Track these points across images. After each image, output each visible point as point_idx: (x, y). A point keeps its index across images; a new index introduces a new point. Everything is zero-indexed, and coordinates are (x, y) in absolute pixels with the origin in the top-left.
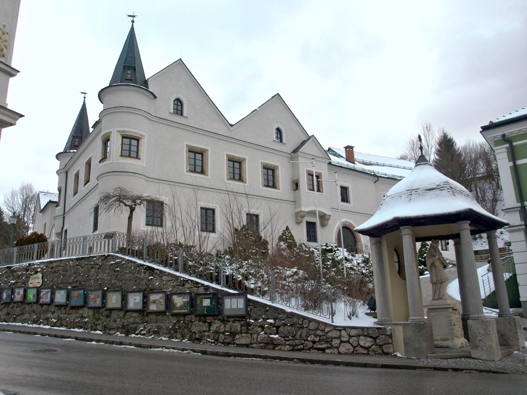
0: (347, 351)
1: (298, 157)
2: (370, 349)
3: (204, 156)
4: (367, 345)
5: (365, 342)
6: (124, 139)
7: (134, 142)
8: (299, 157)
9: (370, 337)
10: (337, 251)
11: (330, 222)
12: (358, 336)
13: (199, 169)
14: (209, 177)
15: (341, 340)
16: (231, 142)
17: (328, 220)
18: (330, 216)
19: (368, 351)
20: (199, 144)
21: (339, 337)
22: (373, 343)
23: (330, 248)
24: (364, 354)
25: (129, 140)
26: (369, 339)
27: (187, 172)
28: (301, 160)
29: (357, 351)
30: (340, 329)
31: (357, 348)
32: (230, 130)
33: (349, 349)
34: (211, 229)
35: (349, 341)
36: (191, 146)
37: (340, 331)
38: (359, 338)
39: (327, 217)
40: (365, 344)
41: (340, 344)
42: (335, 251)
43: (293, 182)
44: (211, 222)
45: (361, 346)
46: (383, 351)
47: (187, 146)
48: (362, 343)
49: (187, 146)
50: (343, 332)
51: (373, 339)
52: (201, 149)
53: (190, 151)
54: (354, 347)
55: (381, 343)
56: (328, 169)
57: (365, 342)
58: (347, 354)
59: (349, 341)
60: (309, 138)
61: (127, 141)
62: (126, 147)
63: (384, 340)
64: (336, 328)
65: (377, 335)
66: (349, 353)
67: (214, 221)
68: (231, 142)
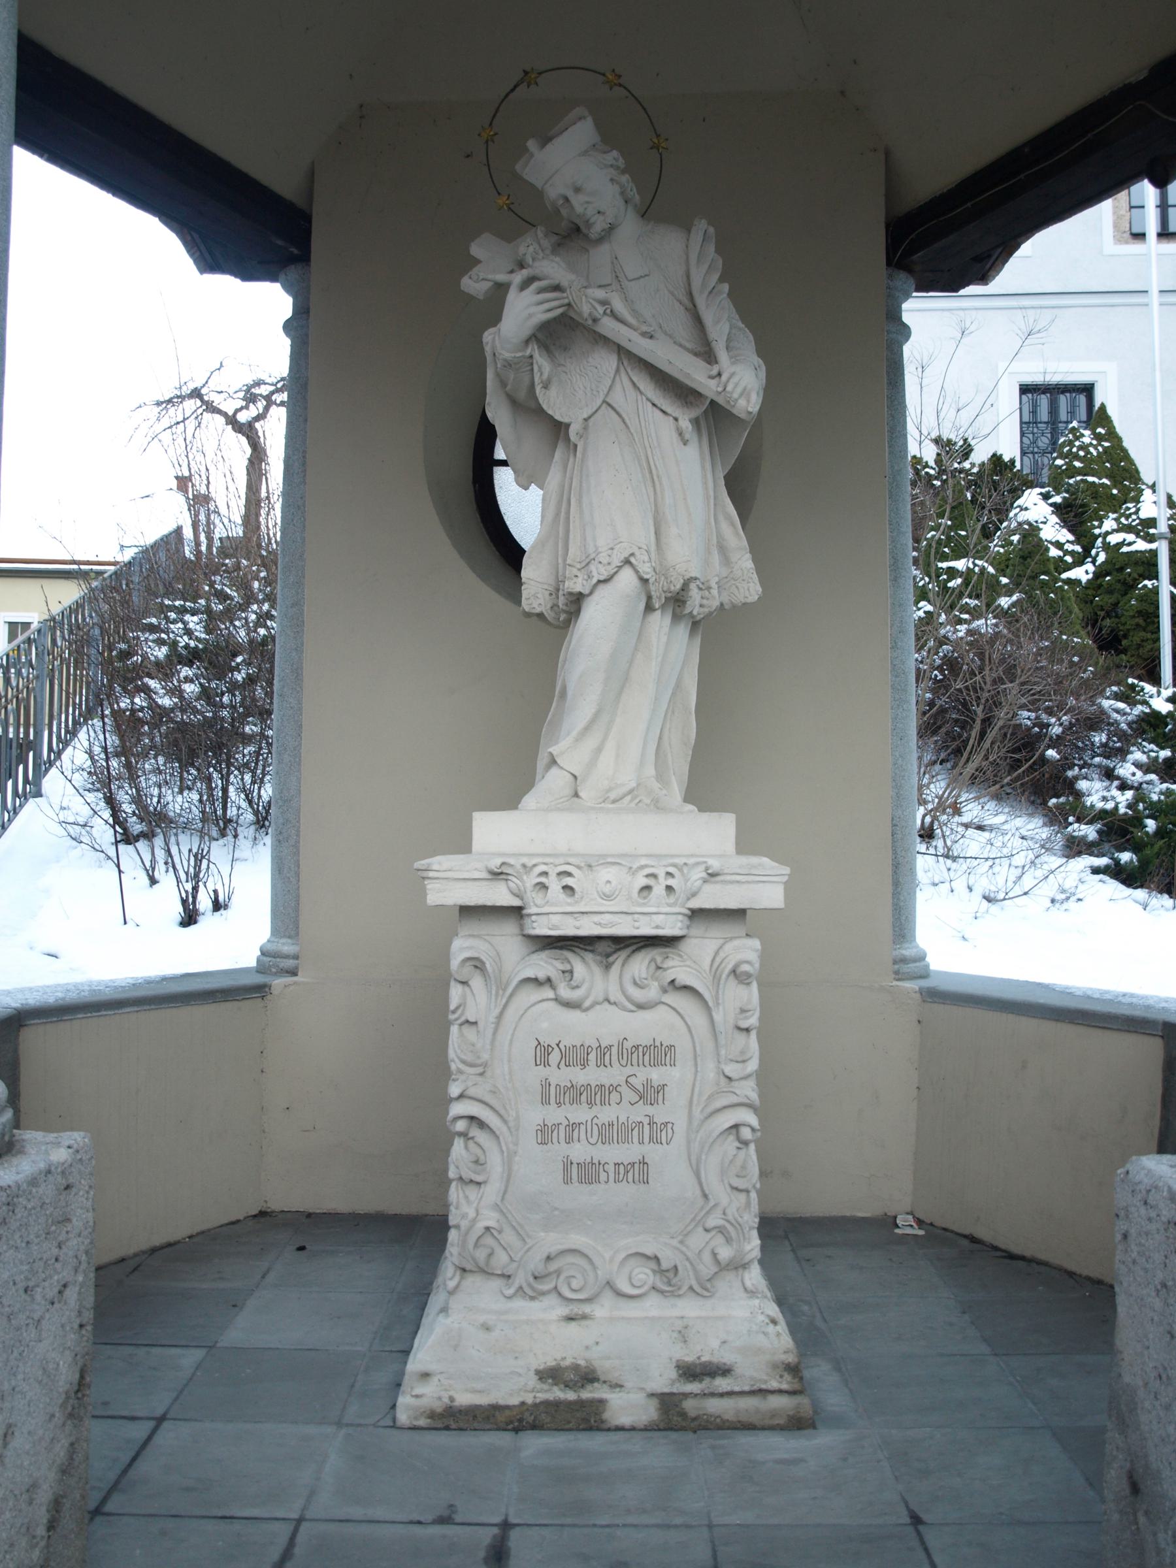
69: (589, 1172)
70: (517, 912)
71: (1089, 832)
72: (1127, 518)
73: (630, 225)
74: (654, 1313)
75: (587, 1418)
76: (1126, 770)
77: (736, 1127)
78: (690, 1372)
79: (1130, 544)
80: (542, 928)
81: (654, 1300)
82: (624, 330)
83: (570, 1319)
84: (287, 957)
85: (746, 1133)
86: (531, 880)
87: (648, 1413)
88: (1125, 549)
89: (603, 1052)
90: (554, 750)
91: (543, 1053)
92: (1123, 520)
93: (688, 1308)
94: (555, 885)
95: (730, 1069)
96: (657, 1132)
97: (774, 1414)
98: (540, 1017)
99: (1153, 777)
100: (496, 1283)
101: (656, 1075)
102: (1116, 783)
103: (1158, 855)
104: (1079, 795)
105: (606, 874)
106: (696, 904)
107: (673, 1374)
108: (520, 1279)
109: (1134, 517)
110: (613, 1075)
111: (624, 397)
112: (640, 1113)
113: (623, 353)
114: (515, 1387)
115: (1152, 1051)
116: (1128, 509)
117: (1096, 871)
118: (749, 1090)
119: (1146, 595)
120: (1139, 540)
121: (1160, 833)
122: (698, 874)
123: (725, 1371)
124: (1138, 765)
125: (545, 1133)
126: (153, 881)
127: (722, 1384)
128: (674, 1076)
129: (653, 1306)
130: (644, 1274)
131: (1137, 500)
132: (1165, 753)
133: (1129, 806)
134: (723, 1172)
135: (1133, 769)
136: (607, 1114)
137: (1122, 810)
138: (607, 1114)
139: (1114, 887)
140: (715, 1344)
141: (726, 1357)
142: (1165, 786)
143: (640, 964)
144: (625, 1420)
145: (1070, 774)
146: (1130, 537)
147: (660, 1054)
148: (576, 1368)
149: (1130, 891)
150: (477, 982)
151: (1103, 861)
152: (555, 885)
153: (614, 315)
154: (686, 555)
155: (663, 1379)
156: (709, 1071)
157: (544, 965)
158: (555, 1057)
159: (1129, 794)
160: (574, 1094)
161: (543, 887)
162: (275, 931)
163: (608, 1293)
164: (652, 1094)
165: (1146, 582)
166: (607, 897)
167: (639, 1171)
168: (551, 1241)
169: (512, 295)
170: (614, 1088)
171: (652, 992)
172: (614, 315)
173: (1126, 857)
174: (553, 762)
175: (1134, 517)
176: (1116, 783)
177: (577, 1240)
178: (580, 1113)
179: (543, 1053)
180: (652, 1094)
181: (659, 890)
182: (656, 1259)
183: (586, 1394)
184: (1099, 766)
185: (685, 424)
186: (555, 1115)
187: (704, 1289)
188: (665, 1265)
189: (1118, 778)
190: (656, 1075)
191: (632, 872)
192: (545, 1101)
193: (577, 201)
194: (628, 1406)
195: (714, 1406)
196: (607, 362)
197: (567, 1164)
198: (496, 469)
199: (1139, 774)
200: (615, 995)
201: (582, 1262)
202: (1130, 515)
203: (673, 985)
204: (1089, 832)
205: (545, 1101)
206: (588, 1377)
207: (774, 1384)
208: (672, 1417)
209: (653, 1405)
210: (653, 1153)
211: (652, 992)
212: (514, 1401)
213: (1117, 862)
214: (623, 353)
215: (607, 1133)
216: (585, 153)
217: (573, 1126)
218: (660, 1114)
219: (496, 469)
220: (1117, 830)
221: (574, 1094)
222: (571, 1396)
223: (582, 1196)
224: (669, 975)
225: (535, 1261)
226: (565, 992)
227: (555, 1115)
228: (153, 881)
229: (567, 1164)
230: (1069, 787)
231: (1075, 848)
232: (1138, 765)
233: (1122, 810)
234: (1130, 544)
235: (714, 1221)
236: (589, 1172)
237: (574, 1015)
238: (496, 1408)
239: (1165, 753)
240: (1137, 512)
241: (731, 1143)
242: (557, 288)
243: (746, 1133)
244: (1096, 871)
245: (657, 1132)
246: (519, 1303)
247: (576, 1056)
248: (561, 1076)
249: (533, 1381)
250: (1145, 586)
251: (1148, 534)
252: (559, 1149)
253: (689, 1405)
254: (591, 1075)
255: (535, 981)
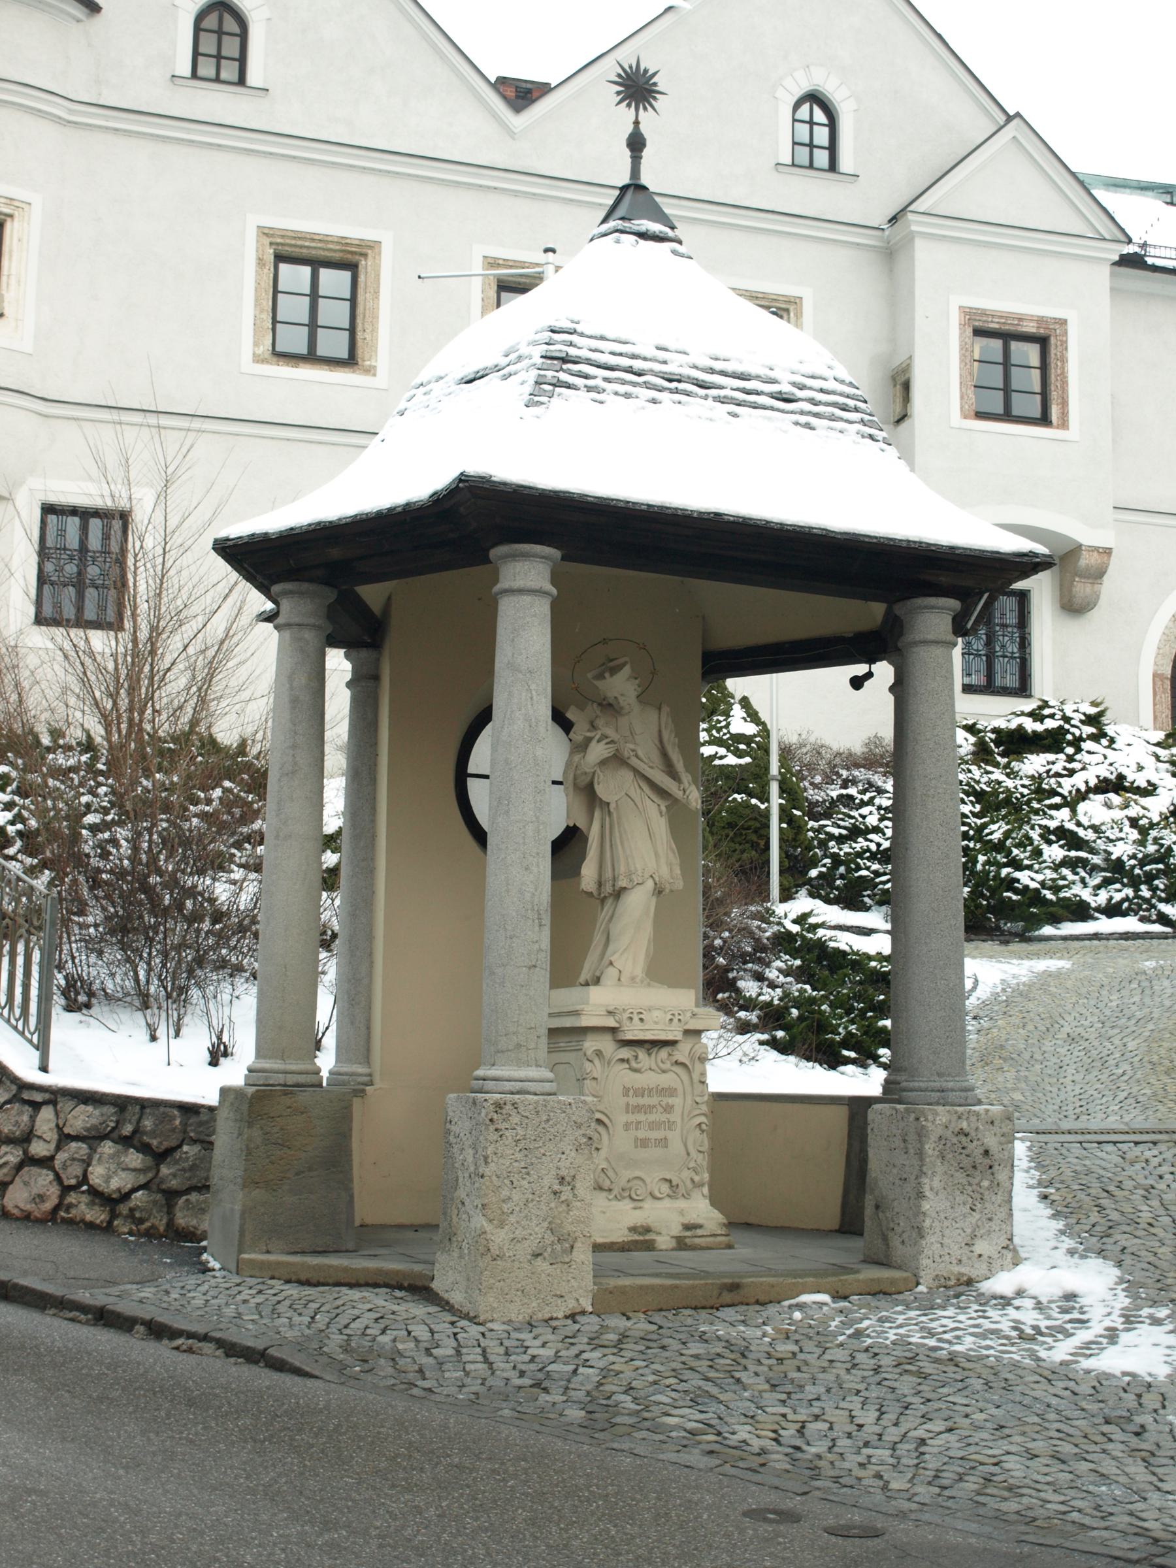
0: (29, 1207)
1: (910, 238)
2: (123, 1209)
3: (1053, 351)
4: (119, 1182)
5: (114, 1170)
6: (283, 267)
7: (334, 281)
8: (919, 243)
9: (145, 1149)
10: (1088, 745)
11: (1109, 587)
12: (93, 1138)
13: (332, 344)
14: (381, 379)
15: (25, 1152)
16: (516, 194)
17: (1098, 574)
18: (1108, 552)
19: (114, 1215)
20: (325, 220)
21: (27, 1138)
22: (142, 1179)
23: (1050, 724)
24: (91, 1226)
25: (306, 271)
26: (134, 1158)
27: (258, 359)
28: (928, 259)
29: (70, 1207)
30: (38, 1097)
31: (72, 1198)
32: (511, 134)
33: (41, 1198)
34: (1012, 681)
35: (52, 1158)
36: (284, 234)
37: (36, 1106)
38: (93, 1149)
39: (1086, 560)
40: (108, 1179)
41: (19, 1167)
42: (1077, 743)
43: (894, 378)
44: (1014, 648)
45: (94, 1192)
46: (170, 1224)
47: (264, 232)
48: (97, 1175)
49: (264, 232)
50: (47, 1113)
51: (149, 1161)
52: (342, 241)
53: (979, 332)
54: (66, 1190)
55: (174, 1183)
56: (1112, 289)
57: (114, 1170)
58: (27, 1217)
59: (52, 1158)
60: (1010, 119)
61: (296, 277)
62: (295, 309)
63: (193, 1168)
64: (26, 1095)
65: (174, 1143)
66: (37, 1214)
67: (1024, 643)
68: (516, 194)
69: (644, 1143)
70: (613, 1030)
71: (753, 1017)
72: (718, 732)
73: (636, 708)
74: (668, 1205)
75: (649, 1246)
76: (772, 974)
77: (699, 1125)
78: (688, 1227)
79: (721, 758)
80: (629, 1036)
81: (667, 1200)
82: (642, 764)
83: (635, 1208)
84: (361, 1075)
85: (704, 1126)
86: (627, 1015)
87: (673, 1244)
88: (717, 762)
89: (650, 1090)
90: (612, 959)
91: (626, 1091)
92: (714, 732)
93: (681, 1204)
94: (636, 1018)
95: (698, 1099)
96: (670, 1125)
97: (720, 1243)
98: (622, 1076)
99: (789, 979)
100: (605, 1194)
101: (670, 1101)
102: (766, 983)
103: (801, 1033)
104: (738, 991)
105: (656, 1013)
106: (687, 1027)
107: (681, 1228)
108: (615, 1192)
109: (725, 731)
110: (653, 1101)
111: (635, 793)
112: (664, 1117)
113: (636, 771)
114: (619, 1235)
115: (843, 1112)
116: (720, 722)
117: (762, 1043)
118: (704, 1108)
119: (735, 808)
120: (729, 754)
121: (801, 1018)
122: (689, 1014)
123: (700, 1227)
124: (780, 970)
125: (627, 1126)
126: (153, 1038)
127: (699, 1232)
128: (677, 1101)
129: (667, 1203)
130: (665, 1188)
131: (727, 715)
132: (798, 962)
133: (780, 999)
134: (695, 1142)
135: (777, 973)
136: (652, 1117)
137: (776, 1002)
138: (652, 1117)
139: (774, 1054)
140: (695, 1216)
141: (700, 1221)
142: (800, 986)
143: (664, 1053)
144: (664, 1247)
145: (731, 975)
146: (722, 751)
147: (671, 1092)
148: (642, 1226)
149: (784, 1057)
150: (596, 1061)
151: (765, 1037)
152: (636, 1018)
153: (637, 756)
154: (664, 871)
155: (676, 1230)
156: (689, 1101)
157: (625, 1053)
158: (631, 1093)
159: (779, 991)
160: (639, 1109)
161: (631, 1019)
162: (338, 1060)
163: (649, 1197)
164: (668, 1109)
165: (736, 796)
166: (656, 1023)
167: (663, 1142)
168: (627, 1174)
169: (594, 743)
170: (654, 1106)
171: (667, 1066)
172: (637, 756)
173: (780, 1034)
174: (611, 963)
175: (725, 731)
176: (766, 983)
177: (638, 1173)
178: (641, 1117)
179: (626, 1091)
180: (668, 1109)
181: (675, 1020)
182: (670, 1181)
183: (647, 1238)
184: (750, 971)
185: (663, 808)
186: (632, 1118)
187: (686, 1196)
188: (674, 1183)
189: (767, 979)
190: (670, 1101)
191: (665, 1012)
192: (627, 1112)
193: (621, 699)
194: (664, 1241)
195: (697, 1241)
196: (629, 776)
197: (636, 1139)
198: (469, 779)
199: (781, 977)
200: (654, 1066)
201: (640, 1183)
202: (721, 728)
203: (676, 1063)
204: (753, 1017)
205: (627, 1112)
206: (648, 1230)
207: (719, 1232)
208: (681, 1244)
209: (674, 1241)
210: (670, 1135)
211: (667, 1066)
212: (620, 1240)
213: (774, 1038)
214: (636, 771)
215: (652, 1126)
216: (628, 679)
217: (639, 1123)
218: (672, 1118)
219: (469, 779)
220: (772, 1017)
221: (639, 1109)
222: (641, 1238)
223: (643, 1154)
224: (675, 1058)
225: (623, 1182)
226: (634, 1065)
227: (632, 1118)
228: (153, 1038)
229: (636, 1139)
230: (732, 986)
231: (744, 1028)
232: (780, 970)
233: (776, 1002)
234: (721, 758)
235: (692, 1165)
236: (644, 1143)
237: (637, 1075)
238: (613, 1243)
239: (798, 962)
240: (727, 726)
241: (698, 1132)
242: (612, 742)
243: (704, 1126)
244: (762, 1043)
245: (670, 1125)
246: (614, 1203)
247: (640, 1093)
248: (634, 1101)
249: (626, 1232)
250: (735, 799)
251: (737, 749)
252: (633, 1133)
253: (687, 1240)
254: (645, 1101)
255: (622, 1060)
